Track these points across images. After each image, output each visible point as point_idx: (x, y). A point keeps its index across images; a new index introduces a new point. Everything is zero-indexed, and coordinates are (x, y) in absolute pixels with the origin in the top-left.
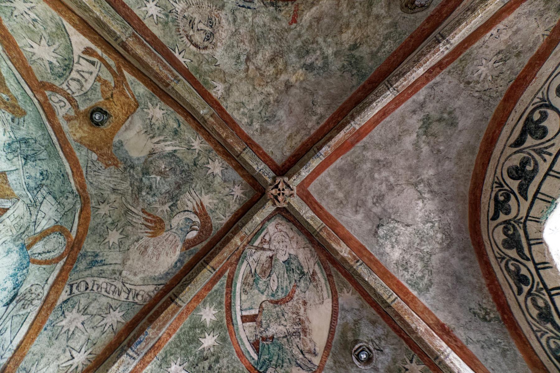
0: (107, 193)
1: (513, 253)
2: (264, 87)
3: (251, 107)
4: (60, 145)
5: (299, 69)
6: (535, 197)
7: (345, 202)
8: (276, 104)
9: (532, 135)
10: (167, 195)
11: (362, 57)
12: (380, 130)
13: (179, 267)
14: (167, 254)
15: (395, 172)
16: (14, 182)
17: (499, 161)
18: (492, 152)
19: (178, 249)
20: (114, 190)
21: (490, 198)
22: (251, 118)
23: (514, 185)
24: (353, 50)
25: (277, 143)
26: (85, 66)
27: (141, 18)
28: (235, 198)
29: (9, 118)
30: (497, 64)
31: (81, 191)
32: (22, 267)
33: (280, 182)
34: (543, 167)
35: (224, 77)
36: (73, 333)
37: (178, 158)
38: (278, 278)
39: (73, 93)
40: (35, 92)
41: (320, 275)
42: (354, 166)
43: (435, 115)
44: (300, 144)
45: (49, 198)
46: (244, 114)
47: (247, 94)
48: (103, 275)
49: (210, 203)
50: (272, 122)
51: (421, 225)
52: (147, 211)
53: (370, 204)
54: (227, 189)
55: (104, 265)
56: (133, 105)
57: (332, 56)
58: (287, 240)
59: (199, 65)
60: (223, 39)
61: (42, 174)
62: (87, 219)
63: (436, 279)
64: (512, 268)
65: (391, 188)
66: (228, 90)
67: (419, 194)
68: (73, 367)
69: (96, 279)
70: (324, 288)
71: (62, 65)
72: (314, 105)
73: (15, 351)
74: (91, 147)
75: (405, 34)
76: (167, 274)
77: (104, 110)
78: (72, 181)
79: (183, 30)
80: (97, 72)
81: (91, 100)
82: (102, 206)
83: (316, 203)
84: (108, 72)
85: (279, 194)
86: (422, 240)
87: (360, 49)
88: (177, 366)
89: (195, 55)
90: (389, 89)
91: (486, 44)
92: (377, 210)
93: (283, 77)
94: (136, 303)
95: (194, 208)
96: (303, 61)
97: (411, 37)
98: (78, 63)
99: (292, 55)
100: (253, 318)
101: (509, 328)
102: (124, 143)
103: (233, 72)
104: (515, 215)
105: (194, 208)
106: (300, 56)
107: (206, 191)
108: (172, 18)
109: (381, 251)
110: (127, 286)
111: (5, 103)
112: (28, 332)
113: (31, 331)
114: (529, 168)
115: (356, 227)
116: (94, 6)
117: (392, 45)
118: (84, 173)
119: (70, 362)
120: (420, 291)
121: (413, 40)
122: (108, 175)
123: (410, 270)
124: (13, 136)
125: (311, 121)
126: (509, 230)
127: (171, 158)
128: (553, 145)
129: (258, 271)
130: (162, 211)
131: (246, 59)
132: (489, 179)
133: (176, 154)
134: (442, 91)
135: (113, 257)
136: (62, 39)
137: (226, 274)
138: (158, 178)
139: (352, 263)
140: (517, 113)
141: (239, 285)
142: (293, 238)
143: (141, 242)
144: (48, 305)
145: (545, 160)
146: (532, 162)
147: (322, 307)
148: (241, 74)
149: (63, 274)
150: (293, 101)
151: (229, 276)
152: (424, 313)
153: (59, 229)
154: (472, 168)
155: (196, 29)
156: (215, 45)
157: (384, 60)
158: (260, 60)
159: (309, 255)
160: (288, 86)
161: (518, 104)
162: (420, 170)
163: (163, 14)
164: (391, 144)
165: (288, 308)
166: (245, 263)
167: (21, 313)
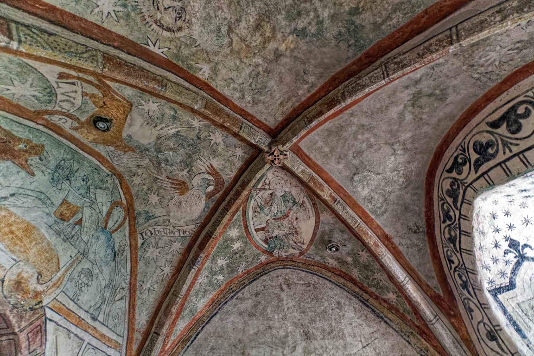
0: (134, 169)
1: (450, 200)
2: (251, 58)
3: (240, 81)
4: (80, 148)
5: (289, 35)
6: (482, 175)
7: (330, 155)
8: (266, 75)
9: (508, 125)
10: (182, 164)
11: (362, 26)
12: (370, 101)
13: (207, 211)
14: (196, 204)
15: (376, 135)
16: (73, 200)
17: (472, 130)
18: (470, 120)
19: (203, 199)
20: (138, 166)
21: (452, 155)
22: (242, 91)
23: (474, 156)
24: (354, 15)
25: (269, 111)
26: (65, 87)
27: (99, 23)
28: (238, 157)
29: (38, 160)
30: (511, 52)
31: (113, 171)
32: (110, 239)
33: (275, 151)
34: (501, 157)
35: (207, 56)
36: (156, 259)
37: (183, 136)
38: (277, 206)
39: (68, 111)
40: (35, 120)
41: (307, 203)
42: (341, 128)
43: (426, 90)
44: (291, 109)
45: (98, 191)
46: (235, 89)
47: (235, 69)
48: (158, 224)
49: (218, 164)
50: (264, 93)
51: (388, 173)
52: (171, 177)
53: (350, 156)
54: (230, 152)
55: (155, 218)
56: (127, 106)
57: (328, 20)
58: (283, 182)
59: (179, 51)
60: (197, 12)
61: (83, 180)
62: (128, 188)
63: (390, 208)
64: (445, 208)
65: (370, 146)
66: (215, 70)
67: (393, 151)
68: (166, 275)
69: (154, 227)
70: (311, 211)
71: (46, 94)
72: (305, 73)
73: (131, 274)
74: (105, 143)
75: (419, 7)
76: (200, 216)
77: (103, 117)
78: (103, 168)
79: (149, 16)
80: (81, 90)
81: (87, 112)
82: (134, 178)
83: (306, 155)
84: (91, 86)
85: (275, 159)
86: (386, 184)
87: (363, 16)
88: (222, 260)
89: (170, 41)
90: (384, 78)
91: (508, 33)
92: (356, 162)
93: (272, 46)
94: (186, 236)
95: (206, 170)
96: (293, 25)
97: (426, 12)
98: (58, 87)
99: (280, 17)
100: (263, 229)
101: (429, 238)
102: (133, 136)
103: (216, 48)
104: (463, 178)
105: (206, 170)
106: (290, 18)
107: (213, 156)
108: (132, 5)
109: (354, 190)
110: (177, 228)
111: (26, 151)
112: (131, 264)
113: (133, 263)
114: (490, 151)
115: (338, 174)
116: (55, 56)
117: (401, 20)
118: (109, 159)
119: (163, 273)
120: (377, 215)
121: (426, 17)
122: (129, 157)
123: (373, 203)
124: (49, 171)
125: (302, 89)
126: (454, 185)
127: (176, 137)
128: (517, 145)
129: (263, 204)
130: (183, 176)
131: (228, 30)
132: (457, 141)
133: (180, 134)
134: (441, 72)
135: (159, 211)
136: (33, 74)
137: (241, 209)
138: (171, 153)
139: (331, 204)
140: (508, 96)
141: (250, 214)
142: (287, 180)
143: (174, 199)
144: (134, 248)
145: (504, 153)
146: (495, 148)
147: (309, 222)
148: (225, 50)
149: (132, 228)
150: (283, 71)
151: (243, 210)
152: (375, 228)
153: (116, 204)
154: (447, 131)
155: (163, 8)
156: (190, 22)
157: (387, 34)
158: (244, 28)
159: (300, 192)
160: (278, 55)
161: (513, 88)
162: (399, 134)
163: (121, 6)
164: (377, 113)
165: (286, 222)
166: (253, 200)
167: (122, 258)
